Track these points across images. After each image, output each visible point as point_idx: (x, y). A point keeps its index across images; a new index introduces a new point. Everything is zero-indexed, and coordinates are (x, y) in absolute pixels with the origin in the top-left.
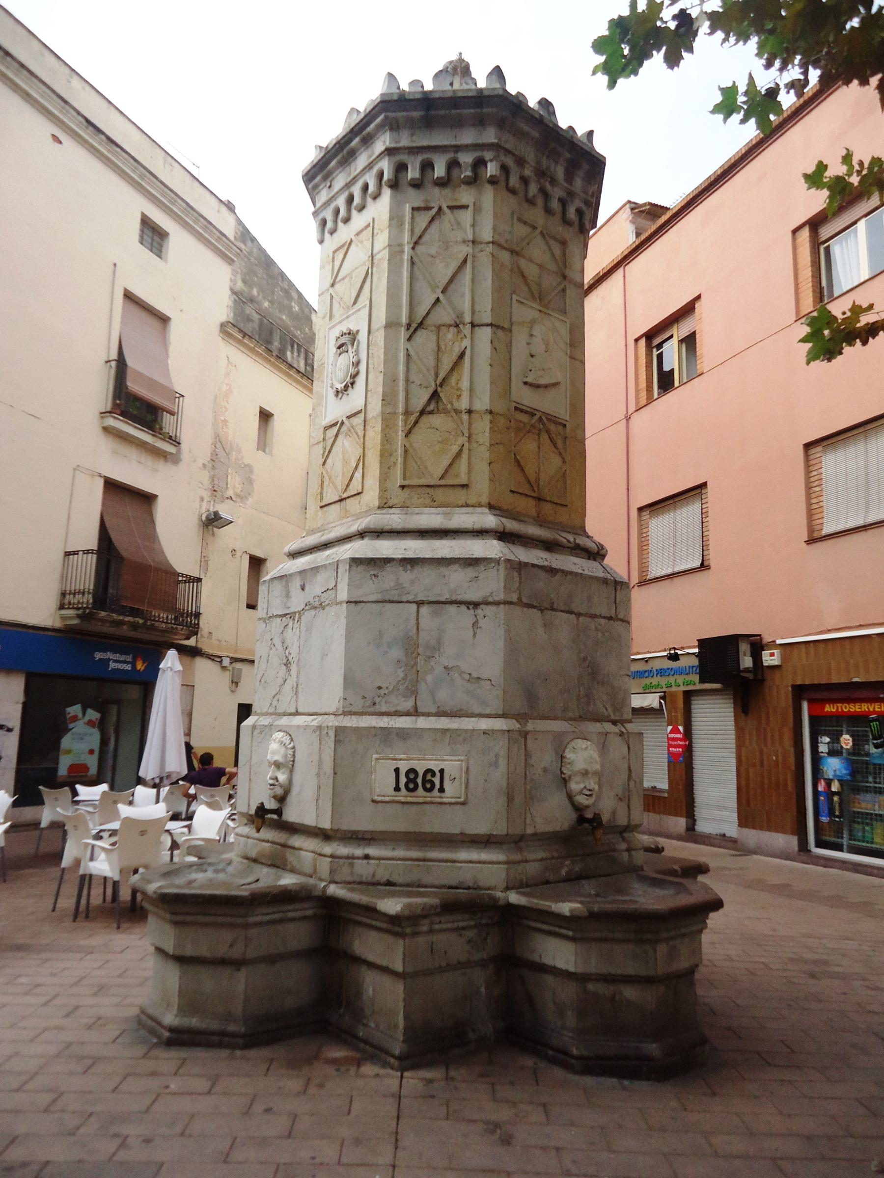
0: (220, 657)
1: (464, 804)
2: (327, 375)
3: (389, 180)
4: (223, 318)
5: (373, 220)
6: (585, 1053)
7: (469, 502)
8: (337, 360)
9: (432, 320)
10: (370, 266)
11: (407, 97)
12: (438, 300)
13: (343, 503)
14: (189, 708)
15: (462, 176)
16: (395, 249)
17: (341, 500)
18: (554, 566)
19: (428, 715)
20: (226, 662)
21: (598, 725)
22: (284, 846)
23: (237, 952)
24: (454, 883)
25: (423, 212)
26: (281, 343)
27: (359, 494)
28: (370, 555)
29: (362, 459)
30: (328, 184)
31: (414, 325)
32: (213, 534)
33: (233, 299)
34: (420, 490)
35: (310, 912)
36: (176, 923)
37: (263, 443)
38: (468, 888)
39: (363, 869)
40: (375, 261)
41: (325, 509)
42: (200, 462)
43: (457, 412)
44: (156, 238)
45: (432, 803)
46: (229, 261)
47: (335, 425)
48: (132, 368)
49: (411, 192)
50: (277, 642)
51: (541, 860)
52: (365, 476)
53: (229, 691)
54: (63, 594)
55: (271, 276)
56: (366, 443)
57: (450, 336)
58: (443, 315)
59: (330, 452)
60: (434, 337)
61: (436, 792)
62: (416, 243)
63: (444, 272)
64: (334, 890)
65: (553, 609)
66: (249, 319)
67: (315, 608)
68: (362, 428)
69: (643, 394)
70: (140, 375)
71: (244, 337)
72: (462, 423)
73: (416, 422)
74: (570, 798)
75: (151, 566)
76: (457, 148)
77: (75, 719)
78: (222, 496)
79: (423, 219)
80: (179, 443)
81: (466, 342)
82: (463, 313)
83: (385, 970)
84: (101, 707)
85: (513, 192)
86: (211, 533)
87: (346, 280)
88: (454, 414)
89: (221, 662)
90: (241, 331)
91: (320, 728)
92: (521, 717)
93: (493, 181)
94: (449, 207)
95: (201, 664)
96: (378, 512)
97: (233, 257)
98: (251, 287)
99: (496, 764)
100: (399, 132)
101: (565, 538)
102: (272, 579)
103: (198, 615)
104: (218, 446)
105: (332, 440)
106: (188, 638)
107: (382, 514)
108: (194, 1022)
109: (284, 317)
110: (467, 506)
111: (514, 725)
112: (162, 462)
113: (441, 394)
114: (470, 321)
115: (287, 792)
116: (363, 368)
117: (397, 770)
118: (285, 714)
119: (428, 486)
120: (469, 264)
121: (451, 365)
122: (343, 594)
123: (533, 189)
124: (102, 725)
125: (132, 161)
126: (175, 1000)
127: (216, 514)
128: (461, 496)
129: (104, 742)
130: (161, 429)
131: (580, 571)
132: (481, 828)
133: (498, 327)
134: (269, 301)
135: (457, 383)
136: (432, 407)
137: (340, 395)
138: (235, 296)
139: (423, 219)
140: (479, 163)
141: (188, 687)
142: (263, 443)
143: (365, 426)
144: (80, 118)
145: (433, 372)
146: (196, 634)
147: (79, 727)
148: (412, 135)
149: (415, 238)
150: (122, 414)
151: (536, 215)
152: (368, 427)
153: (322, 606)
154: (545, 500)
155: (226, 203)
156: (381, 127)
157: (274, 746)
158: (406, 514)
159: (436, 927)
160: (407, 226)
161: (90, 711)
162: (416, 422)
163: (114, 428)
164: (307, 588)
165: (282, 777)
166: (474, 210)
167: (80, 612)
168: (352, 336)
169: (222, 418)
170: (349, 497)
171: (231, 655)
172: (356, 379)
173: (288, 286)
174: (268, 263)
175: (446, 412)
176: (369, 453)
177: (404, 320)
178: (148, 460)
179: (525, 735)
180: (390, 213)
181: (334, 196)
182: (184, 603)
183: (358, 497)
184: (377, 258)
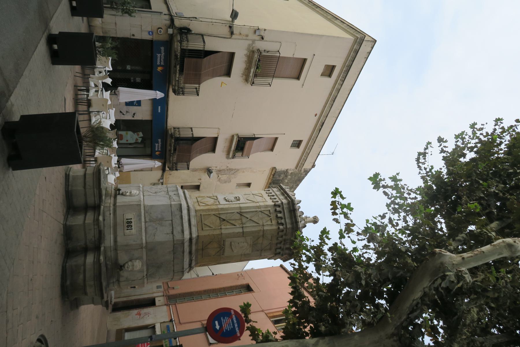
0: (163, 179)
1: (124, 235)
4: (277, 168)
6: (67, 266)
7: (199, 231)
12: (248, 218)
14: (144, 170)
17: (198, 202)
18: (185, 253)
19: (145, 225)
20: (161, 181)
21: (146, 270)
22: (111, 196)
23: (87, 187)
24: (105, 234)
27: (199, 205)
28: (183, 208)
29: (208, 205)
31: (241, 213)
32: (205, 172)
34: (201, 219)
35: (96, 202)
36: (94, 173)
37: (239, 185)
38: (104, 238)
39: (107, 214)
42: (228, 165)
44: (297, 145)
45: (124, 227)
47: (217, 198)
48: (253, 142)
49: (274, 209)
50: (161, 190)
51: (111, 256)
53: (151, 182)
54: (178, 128)
55: (296, 182)
57: (239, 222)
58: (244, 220)
60: (238, 218)
61: (127, 228)
62: (261, 212)
63: (255, 219)
64: (102, 207)
65: (174, 254)
66: (279, 176)
67: (170, 197)
69: (272, 315)
70: (252, 145)
73: (217, 216)
74: (127, 262)
75: (190, 153)
76: (285, 218)
77: (138, 135)
79: (267, 213)
80: (233, 158)
81: (238, 226)
83: (85, 220)
84: (142, 142)
85: (278, 233)
89: (161, 179)
90: (274, 174)
91: (140, 201)
92: (146, 247)
93: (279, 228)
94: (271, 218)
95: (160, 173)
98: (290, 175)
99: (134, 241)
102: (177, 188)
103: (177, 170)
104: (235, 171)
106: (168, 167)
108: (71, 179)
110: (198, 230)
111: (144, 245)
112: (226, 153)
115: (125, 195)
116: (231, 203)
117: (131, 219)
118: (143, 193)
120: (257, 225)
122: (172, 203)
123: (280, 239)
124: (136, 143)
125: (316, 136)
126: (75, 174)
127: (212, 172)
128: (200, 229)
129: (130, 144)
130: (237, 152)
131: (185, 260)
132: (119, 239)
136: (221, 219)
139: (267, 213)
140: (282, 224)
141: (151, 169)
142: (239, 185)
144: (324, 121)
145: (230, 219)
146: (170, 170)
147: (135, 136)
149: (263, 211)
150: (238, 140)
151: (275, 241)
153: (170, 199)
156: (288, 200)
157: (135, 191)
159: (96, 230)
160: (265, 209)
161: (141, 139)
162: (217, 216)
163: (234, 138)
164: (174, 195)
165: (128, 194)
167: (173, 134)
168: (239, 200)
169: (245, 171)
171: (164, 182)
174: (300, 180)
175: (220, 223)
176: (209, 206)
177: (242, 211)
178: (226, 149)
179: (142, 248)
182: (179, 165)
184: (258, 203)
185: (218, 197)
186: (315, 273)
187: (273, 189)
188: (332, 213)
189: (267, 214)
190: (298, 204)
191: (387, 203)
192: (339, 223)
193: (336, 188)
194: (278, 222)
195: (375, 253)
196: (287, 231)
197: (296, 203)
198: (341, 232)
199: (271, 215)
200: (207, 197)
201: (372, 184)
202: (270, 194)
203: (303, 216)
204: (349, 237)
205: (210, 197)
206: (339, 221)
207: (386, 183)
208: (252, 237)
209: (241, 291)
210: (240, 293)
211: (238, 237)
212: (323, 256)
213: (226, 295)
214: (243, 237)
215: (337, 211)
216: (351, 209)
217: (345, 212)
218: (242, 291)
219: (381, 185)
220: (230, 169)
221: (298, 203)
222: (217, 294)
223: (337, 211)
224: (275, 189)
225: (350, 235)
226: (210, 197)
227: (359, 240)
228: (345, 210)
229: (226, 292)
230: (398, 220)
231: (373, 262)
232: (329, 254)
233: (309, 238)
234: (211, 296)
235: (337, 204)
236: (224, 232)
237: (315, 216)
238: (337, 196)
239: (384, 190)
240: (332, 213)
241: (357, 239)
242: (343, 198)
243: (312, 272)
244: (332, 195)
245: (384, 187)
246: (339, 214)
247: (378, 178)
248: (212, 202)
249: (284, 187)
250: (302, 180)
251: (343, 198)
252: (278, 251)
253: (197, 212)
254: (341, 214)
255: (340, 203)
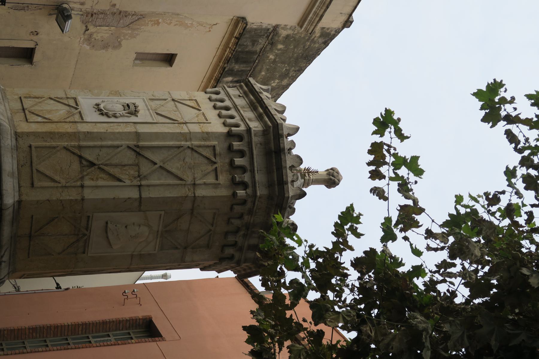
2: (113, 99)
3: (231, 130)
4: (250, 19)
5: (210, 123)
7: (22, 189)
8: (120, 104)
9: (143, 162)
10: (179, 122)
11: (281, 139)
12: (155, 164)
13: (22, 111)
15: (236, 176)
16: (188, 136)
17: (24, 110)
25: (213, 152)
26: (238, 71)
27: (27, 120)
29: (51, 122)
30: (241, 95)
31: (138, 150)
32: (50, 14)
33: (269, 27)
40: (182, 125)
41: (19, 100)
43: (82, 178)
46: (301, 24)
47: (77, 104)
49: (226, 145)
52: (39, 124)
56: (60, 124)
57: (132, 172)
58: (146, 168)
59: (58, 102)
60: (130, 162)
63: (174, 167)
66: (254, 42)
68: (71, 121)
71: (236, 37)
72: (74, 182)
73: (74, 153)
76: (252, 171)
78: (88, 22)
79: (208, 153)
81: (128, 182)
82: (147, 179)
85: (232, 208)
86: (52, 12)
87: (175, 108)
88: (80, 176)
90: (241, 35)
93: (234, 194)
94: (216, 169)
96: (12, 132)
97: (305, 26)
98: (283, 43)
100: (262, 136)
101: (4, 254)
105: (67, 103)
107: (11, 134)
109: (263, 73)
113: (93, 168)
114: (142, 184)
119: (31, 162)
121: (113, 173)
123: (237, 222)
127: (69, 17)
133: (140, 202)
134: (275, 59)
135: (101, 178)
136: (85, 163)
137: (96, 107)
138: (272, 29)
139: (208, 153)
140: (244, 185)
143: (72, 122)
148: (261, 144)
152: (71, 124)
154: (30, 241)
155: (350, 20)
158: (12, 149)
160: (203, 143)
162: (74, 153)
166: (215, 184)
168: (135, 113)
169: (160, 21)
170: (25, 114)
172: (105, 116)
173: (292, 76)
177: (141, 143)
180: (212, 132)
181: (231, 98)
183: (25, 120)
184: (184, 126)
185: (80, 100)
186: (311, 323)
187: (228, 89)
188: (370, 172)
189: (208, 155)
190: (289, 135)
191: (507, 168)
192: (386, 199)
193: (386, 110)
194: (233, 179)
195: (466, 285)
196: (254, 204)
197: (285, 132)
198: (387, 225)
199: (218, 160)
200: (51, 98)
201: (482, 108)
202: (219, 104)
203: (302, 167)
204: (406, 238)
205: (57, 100)
206: (386, 195)
207: (515, 109)
208: (163, 213)
209: (129, 334)
210: (127, 339)
211: (125, 211)
212: (338, 278)
213: (90, 342)
214: (140, 211)
215: (384, 169)
216: (419, 172)
217: (403, 177)
218: (132, 335)
219: (503, 113)
220: (120, 12)
221: (291, 133)
222: (67, 339)
223: (384, 169)
224: (233, 92)
225: (409, 234)
226: (57, 100)
227: (429, 248)
228: (403, 171)
229: (90, 336)
230: (533, 206)
231: (458, 300)
232: (353, 276)
233: (303, 239)
234: (49, 343)
235: (385, 152)
236: (92, 196)
237: (332, 169)
238: (389, 130)
239: (509, 127)
240: (370, 172)
241: (426, 246)
242: (401, 137)
243: (304, 320)
244: (375, 128)
245: (510, 119)
246: (387, 179)
247: (497, 94)
248: (62, 112)
249: (258, 86)
250: (314, 58)
251: (401, 137)
252: (229, 251)
253: (20, 139)
254: (391, 179)
255: (392, 151)
